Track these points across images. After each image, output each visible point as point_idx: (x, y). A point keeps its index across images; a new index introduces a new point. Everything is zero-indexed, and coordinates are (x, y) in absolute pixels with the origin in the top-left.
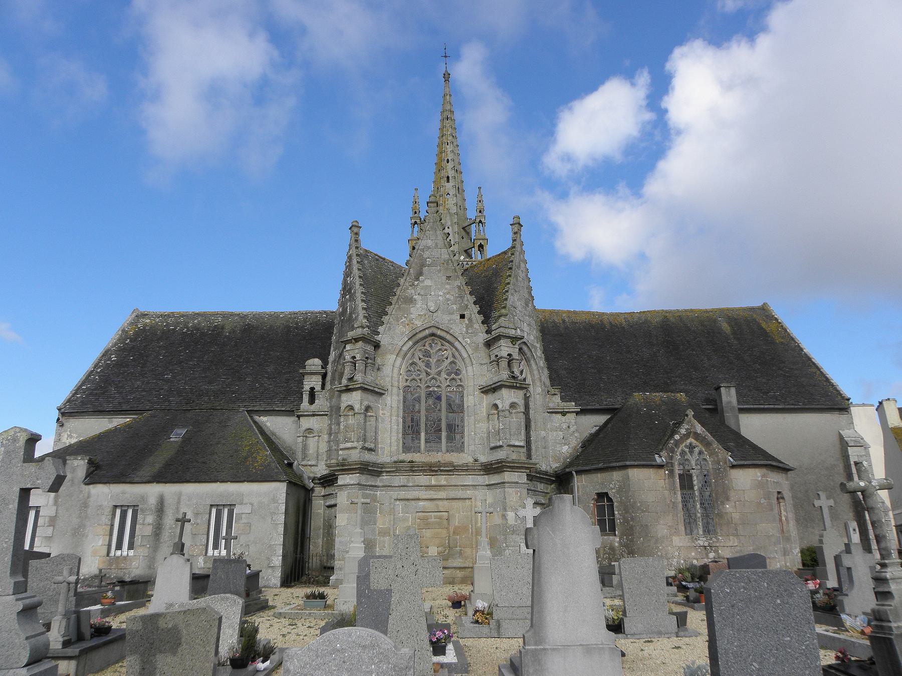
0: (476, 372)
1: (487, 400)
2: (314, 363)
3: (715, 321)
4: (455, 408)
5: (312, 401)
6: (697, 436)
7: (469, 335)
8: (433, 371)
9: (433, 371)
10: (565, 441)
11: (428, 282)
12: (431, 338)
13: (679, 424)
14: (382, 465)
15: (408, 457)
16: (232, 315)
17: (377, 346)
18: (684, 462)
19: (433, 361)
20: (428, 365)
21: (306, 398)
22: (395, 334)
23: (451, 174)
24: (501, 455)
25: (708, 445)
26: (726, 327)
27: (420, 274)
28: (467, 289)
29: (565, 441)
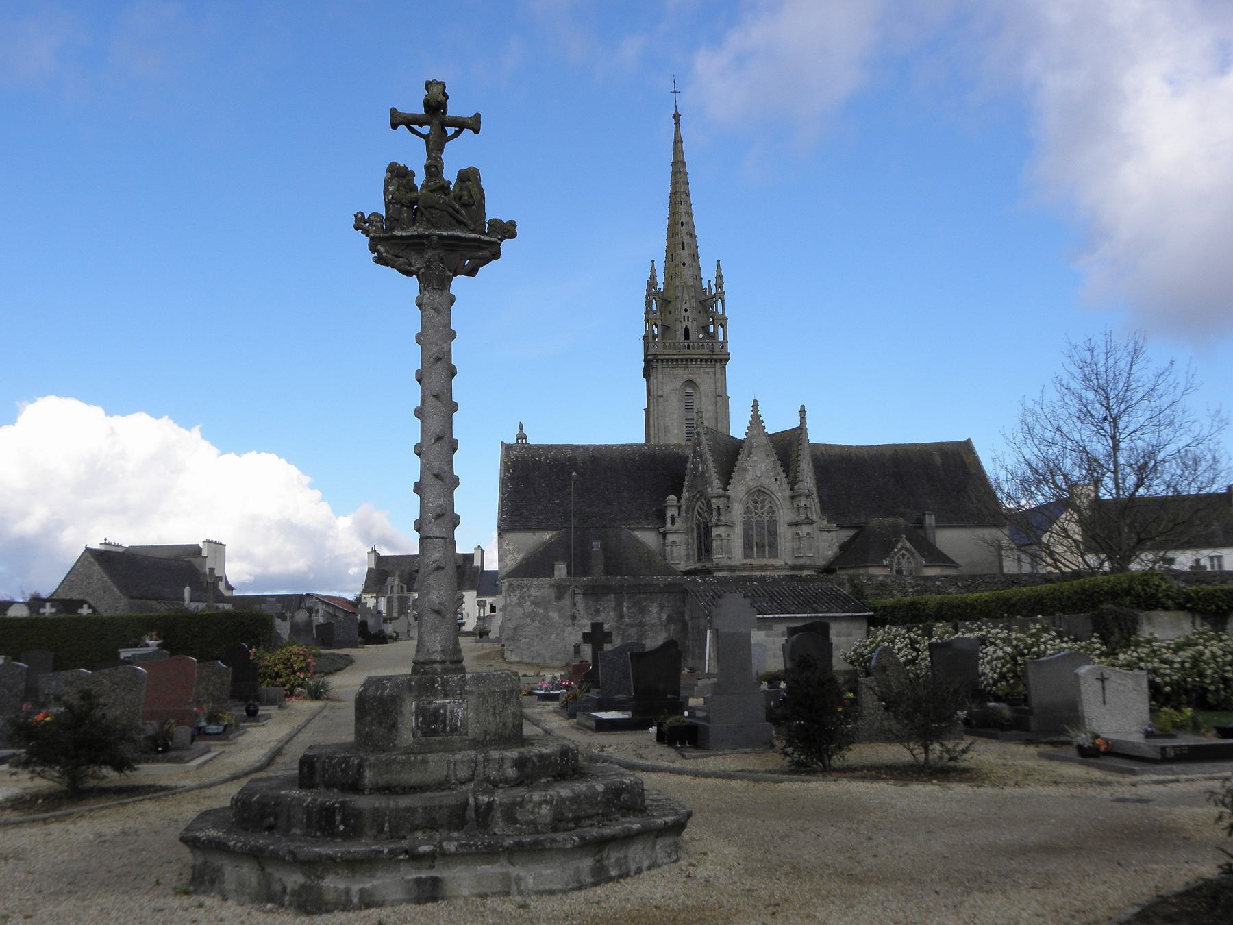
0: (785, 514)
1: (794, 529)
2: (672, 498)
3: (931, 454)
4: (773, 534)
5: (673, 523)
6: (906, 549)
7: (780, 492)
8: (759, 512)
9: (759, 512)
10: (830, 548)
11: (755, 459)
12: (759, 494)
13: (897, 542)
14: (737, 566)
15: (748, 561)
16: (577, 447)
17: (728, 497)
18: (899, 563)
19: (759, 506)
20: (756, 508)
21: (669, 521)
22: (738, 490)
23: (686, 239)
24: (801, 562)
25: (912, 554)
26: (938, 459)
27: (750, 453)
28: (779, 463)
29: (830, 548)
